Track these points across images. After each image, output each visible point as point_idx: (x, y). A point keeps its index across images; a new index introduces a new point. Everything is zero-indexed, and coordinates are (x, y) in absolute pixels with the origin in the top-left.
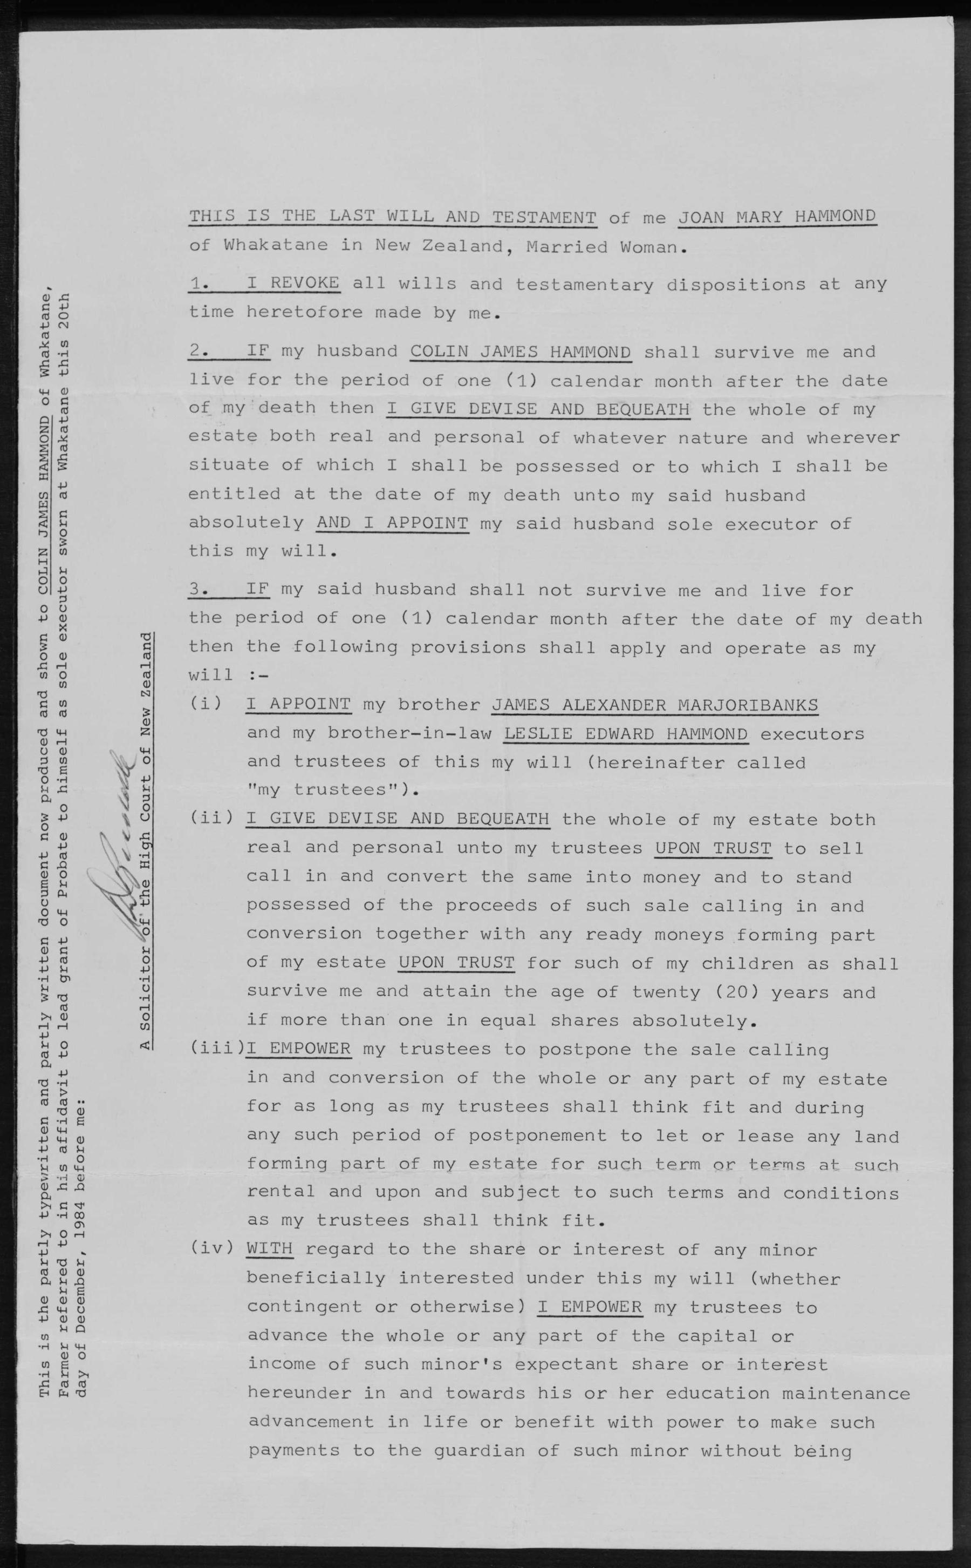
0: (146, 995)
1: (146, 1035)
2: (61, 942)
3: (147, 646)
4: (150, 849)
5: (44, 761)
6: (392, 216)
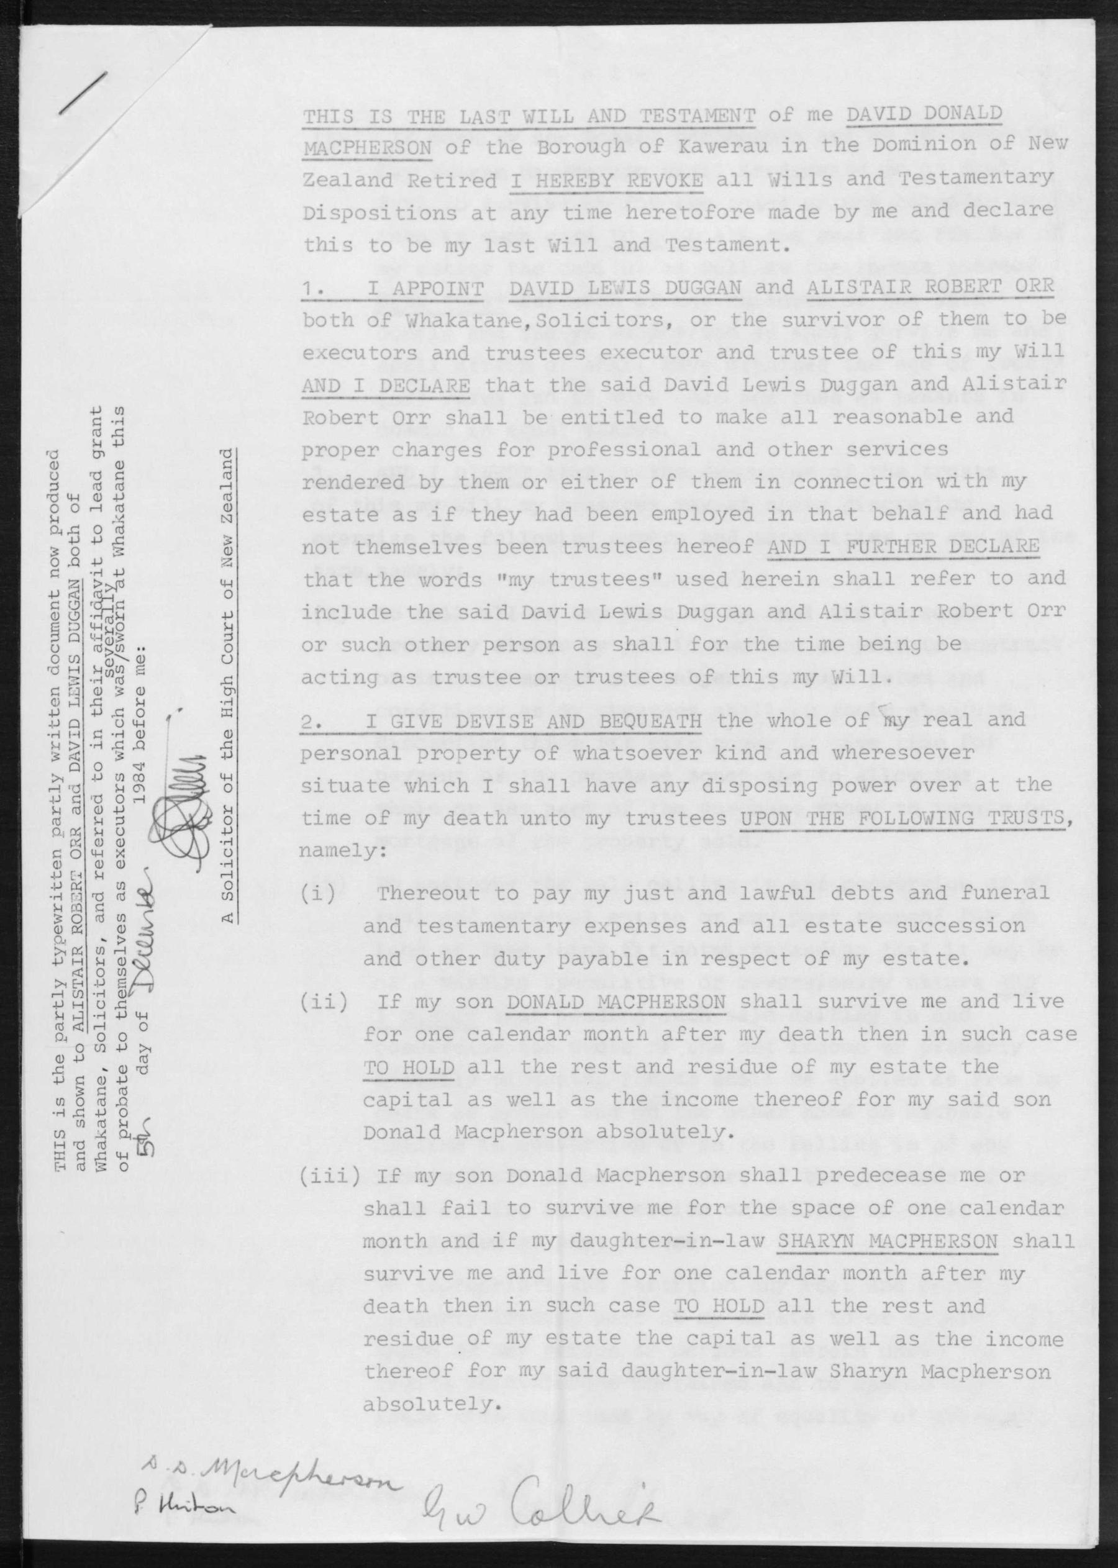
0: (228, 860)
1: (231, 906)
2: (773, 242)
3: (227, 464)
4: (234, 696)
5: (55, 487)
6: (530, 120)
